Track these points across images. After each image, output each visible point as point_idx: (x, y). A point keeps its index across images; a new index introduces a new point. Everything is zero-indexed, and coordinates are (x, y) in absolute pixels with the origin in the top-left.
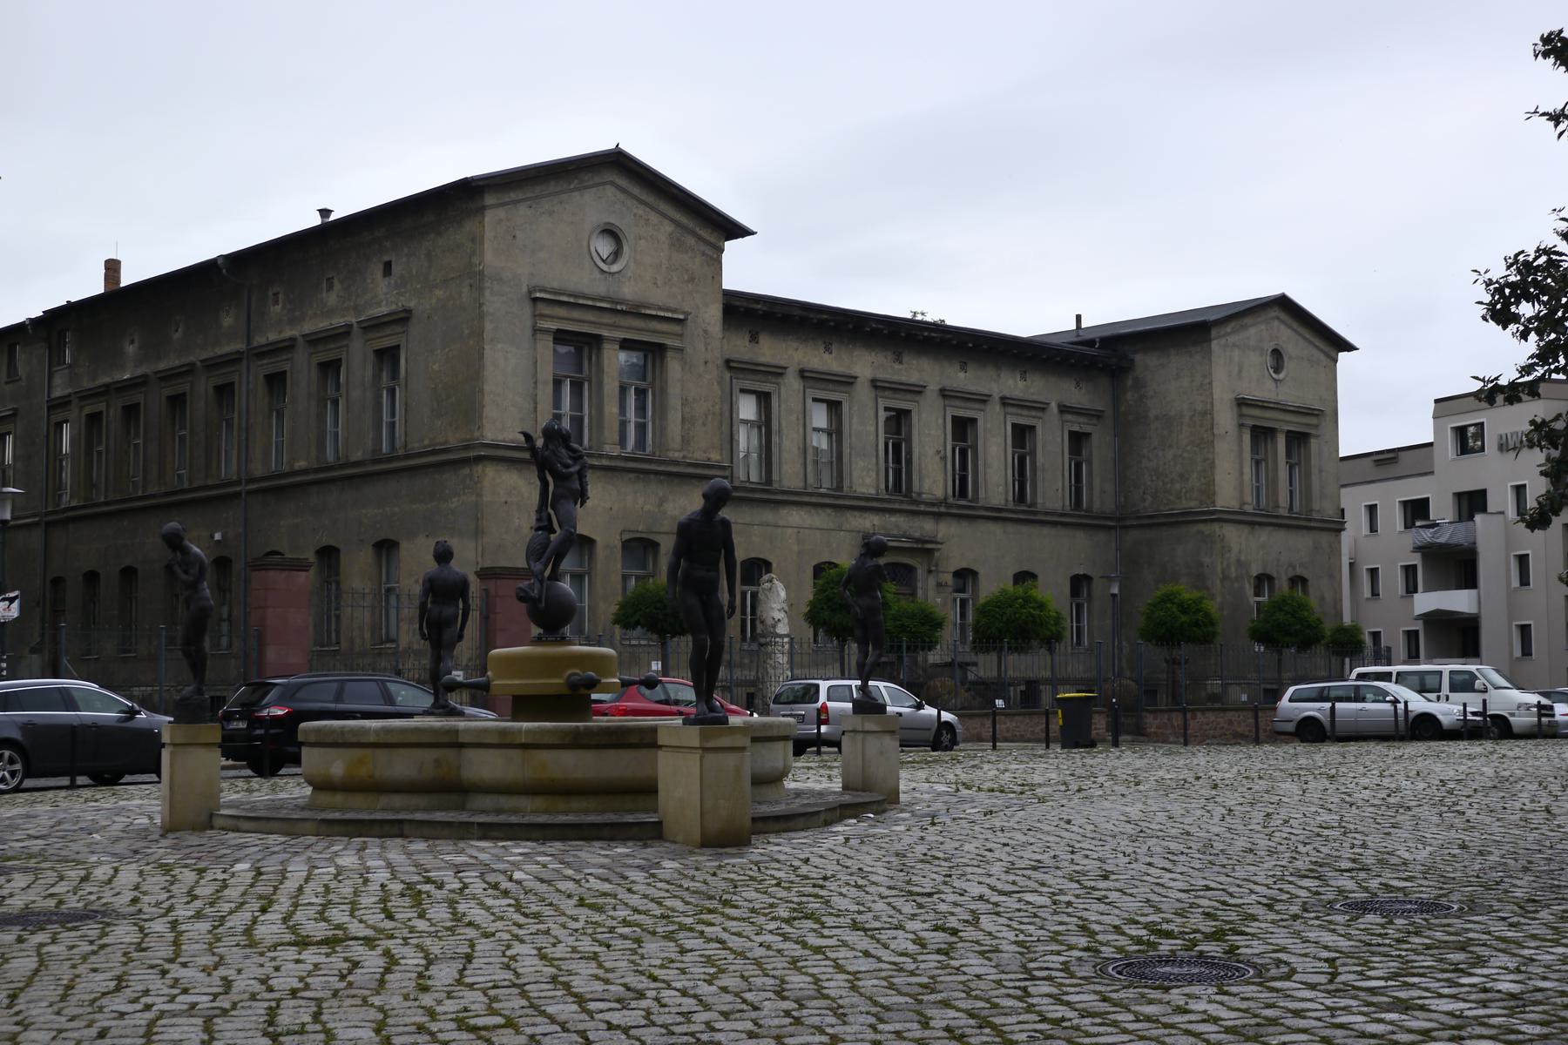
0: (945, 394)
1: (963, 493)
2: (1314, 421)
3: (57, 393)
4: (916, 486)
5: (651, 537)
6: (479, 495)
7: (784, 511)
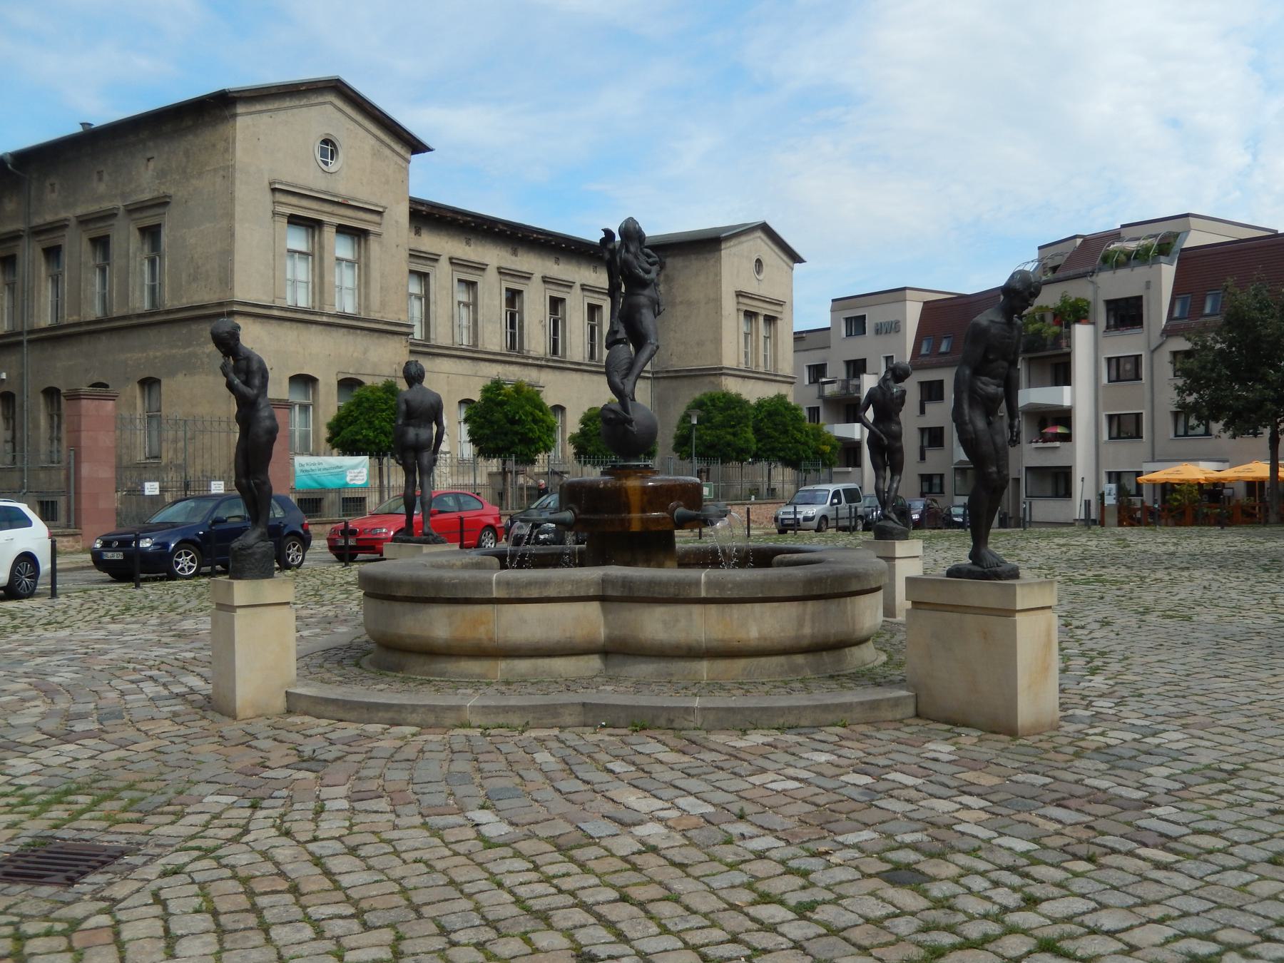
0: (546, 280)
1: (555, 352)
2: (778, 308)
4: (526, 346)
5: (359, 377)
7: (439, 361)
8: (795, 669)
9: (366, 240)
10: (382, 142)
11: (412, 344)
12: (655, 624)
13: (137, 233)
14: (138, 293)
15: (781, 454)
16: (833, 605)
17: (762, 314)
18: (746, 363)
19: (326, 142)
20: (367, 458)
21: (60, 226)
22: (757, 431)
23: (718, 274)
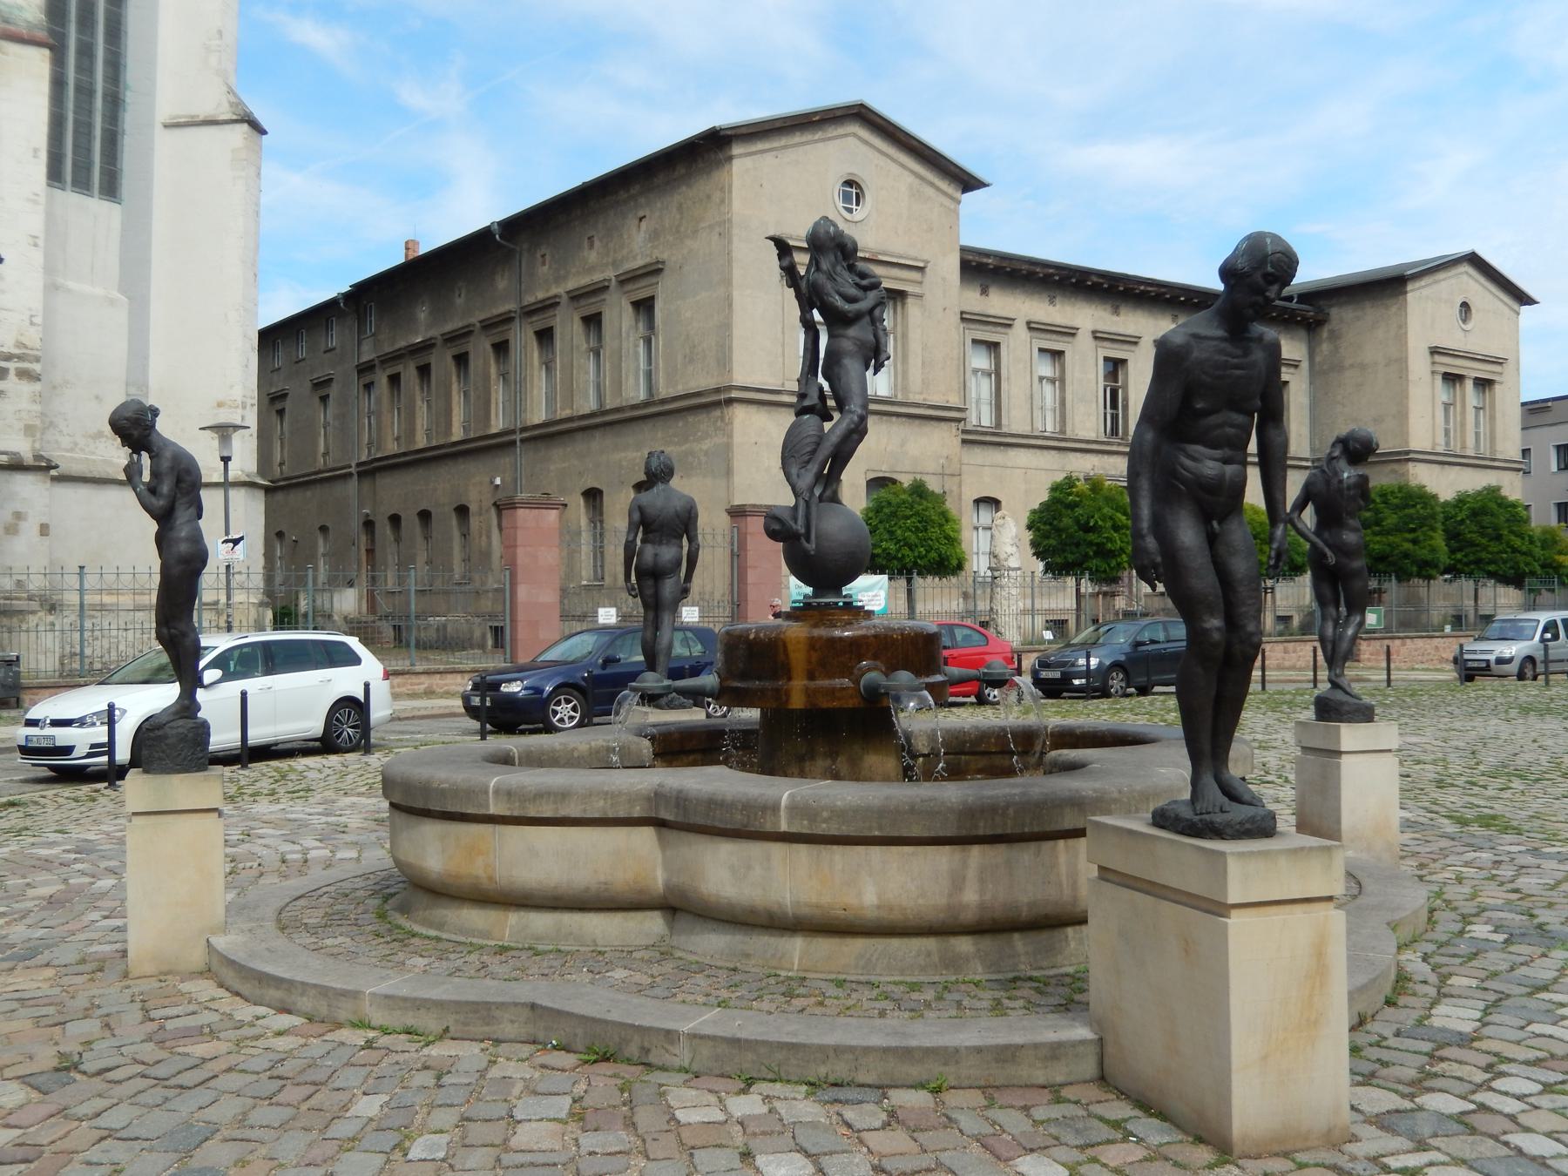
1: (1114, 431)
3: (365, 358)
5: (894, 476)
6: (730, 436)
8: (952, 963)
9: (903, 304)
10: (922, 178)
11: (964, 432)
12: (722, 871)
13: (630, 309)
14: (631, 381)
15: (1491, 568)
16: (1025, 855)
17: (1467, 376)
18: (1447, 444)
19: (849, 183)
20: (883, 579)
21: (549, 305)
22: (1453, 536)
23: (1402, 326)
